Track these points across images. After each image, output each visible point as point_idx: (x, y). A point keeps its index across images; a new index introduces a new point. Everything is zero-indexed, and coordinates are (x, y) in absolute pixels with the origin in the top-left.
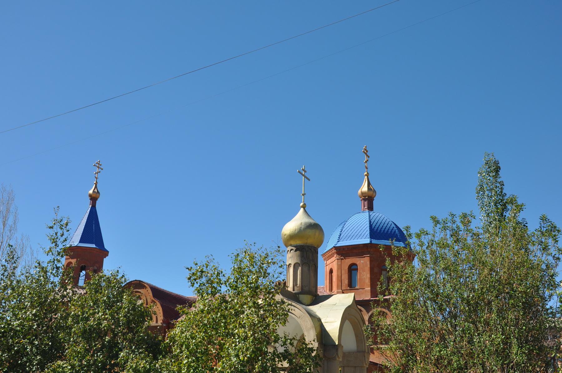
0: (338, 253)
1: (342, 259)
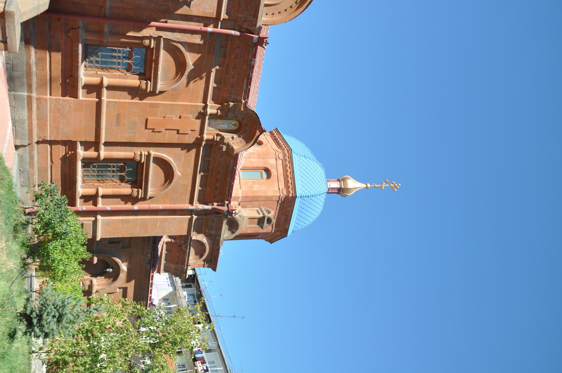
0: (287, 198)
1: (278, 201)
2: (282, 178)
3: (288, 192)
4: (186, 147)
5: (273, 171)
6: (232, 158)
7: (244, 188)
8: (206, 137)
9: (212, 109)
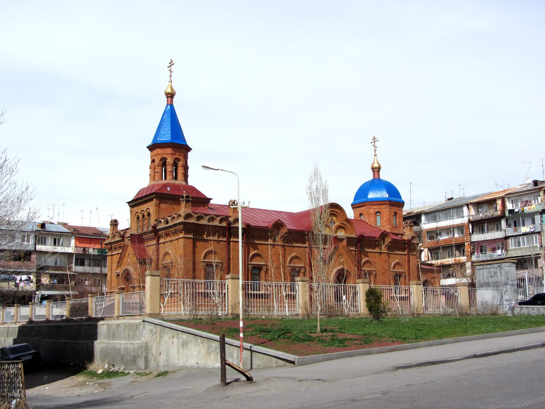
2: (380, 207)
3: (387, 204)
4: (194, 247)
5: (377, 210)
6: (290, 232)
7: (385, 224)
8: (282, 244)
9: (270, 242)
